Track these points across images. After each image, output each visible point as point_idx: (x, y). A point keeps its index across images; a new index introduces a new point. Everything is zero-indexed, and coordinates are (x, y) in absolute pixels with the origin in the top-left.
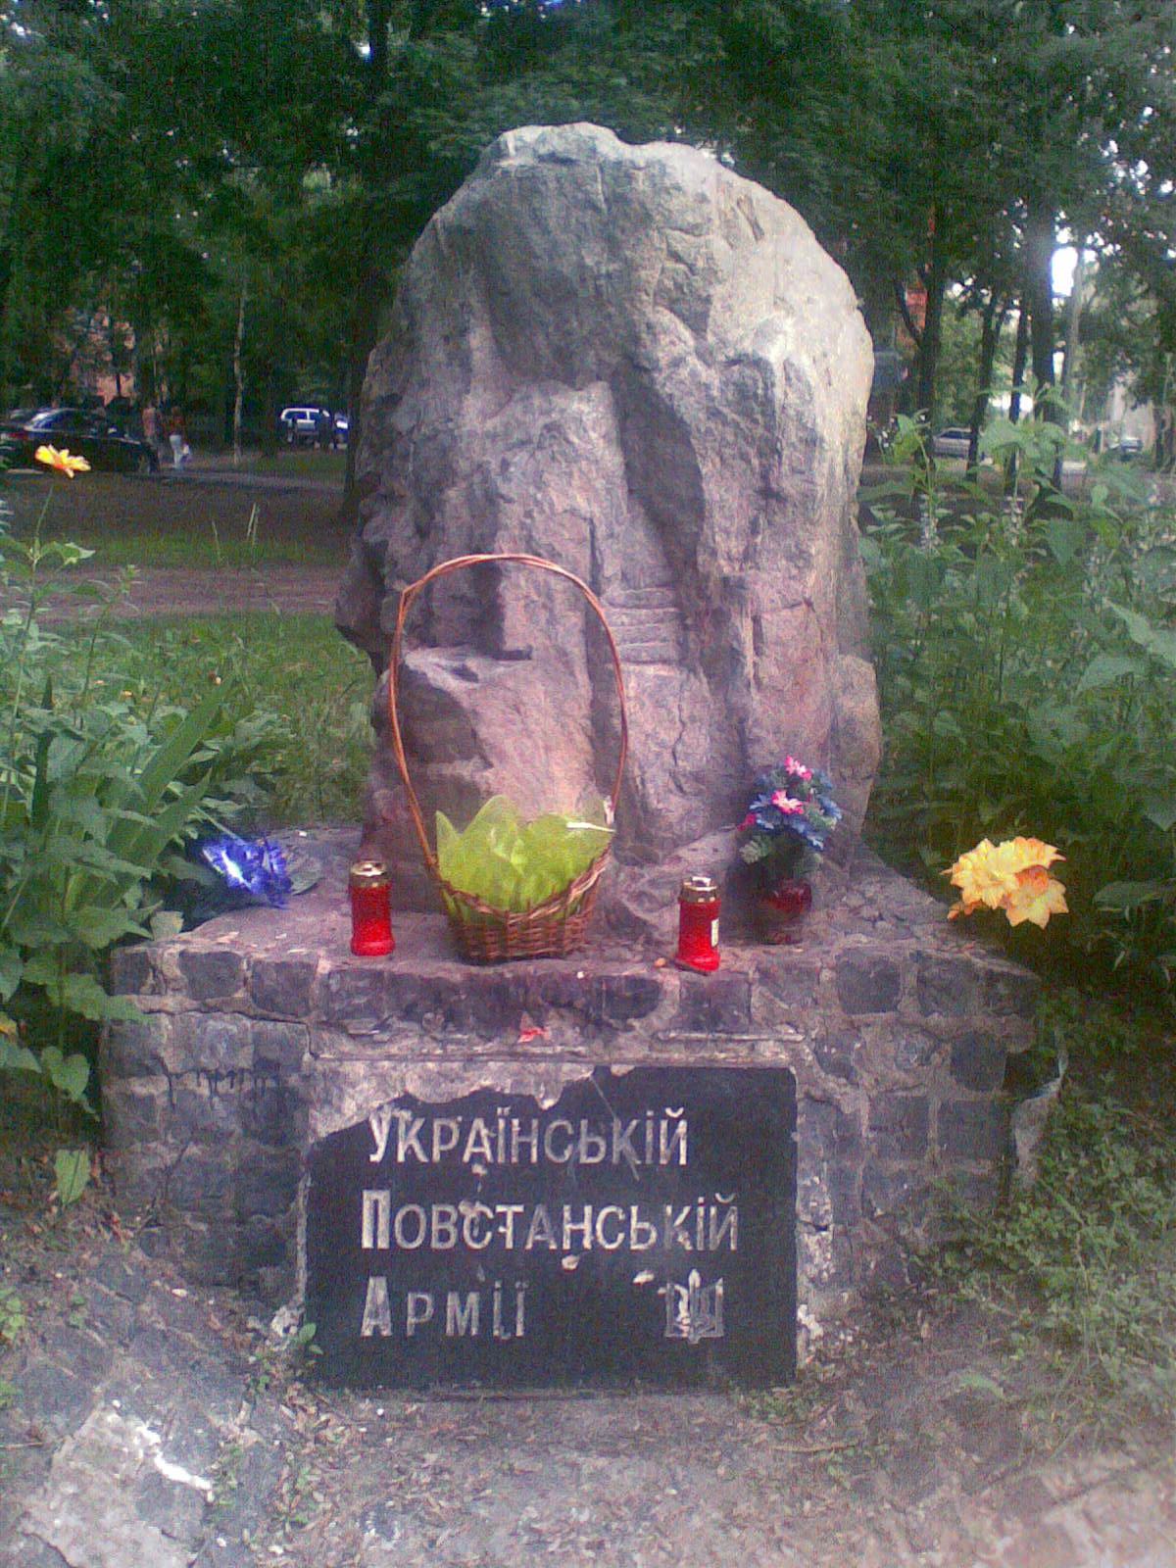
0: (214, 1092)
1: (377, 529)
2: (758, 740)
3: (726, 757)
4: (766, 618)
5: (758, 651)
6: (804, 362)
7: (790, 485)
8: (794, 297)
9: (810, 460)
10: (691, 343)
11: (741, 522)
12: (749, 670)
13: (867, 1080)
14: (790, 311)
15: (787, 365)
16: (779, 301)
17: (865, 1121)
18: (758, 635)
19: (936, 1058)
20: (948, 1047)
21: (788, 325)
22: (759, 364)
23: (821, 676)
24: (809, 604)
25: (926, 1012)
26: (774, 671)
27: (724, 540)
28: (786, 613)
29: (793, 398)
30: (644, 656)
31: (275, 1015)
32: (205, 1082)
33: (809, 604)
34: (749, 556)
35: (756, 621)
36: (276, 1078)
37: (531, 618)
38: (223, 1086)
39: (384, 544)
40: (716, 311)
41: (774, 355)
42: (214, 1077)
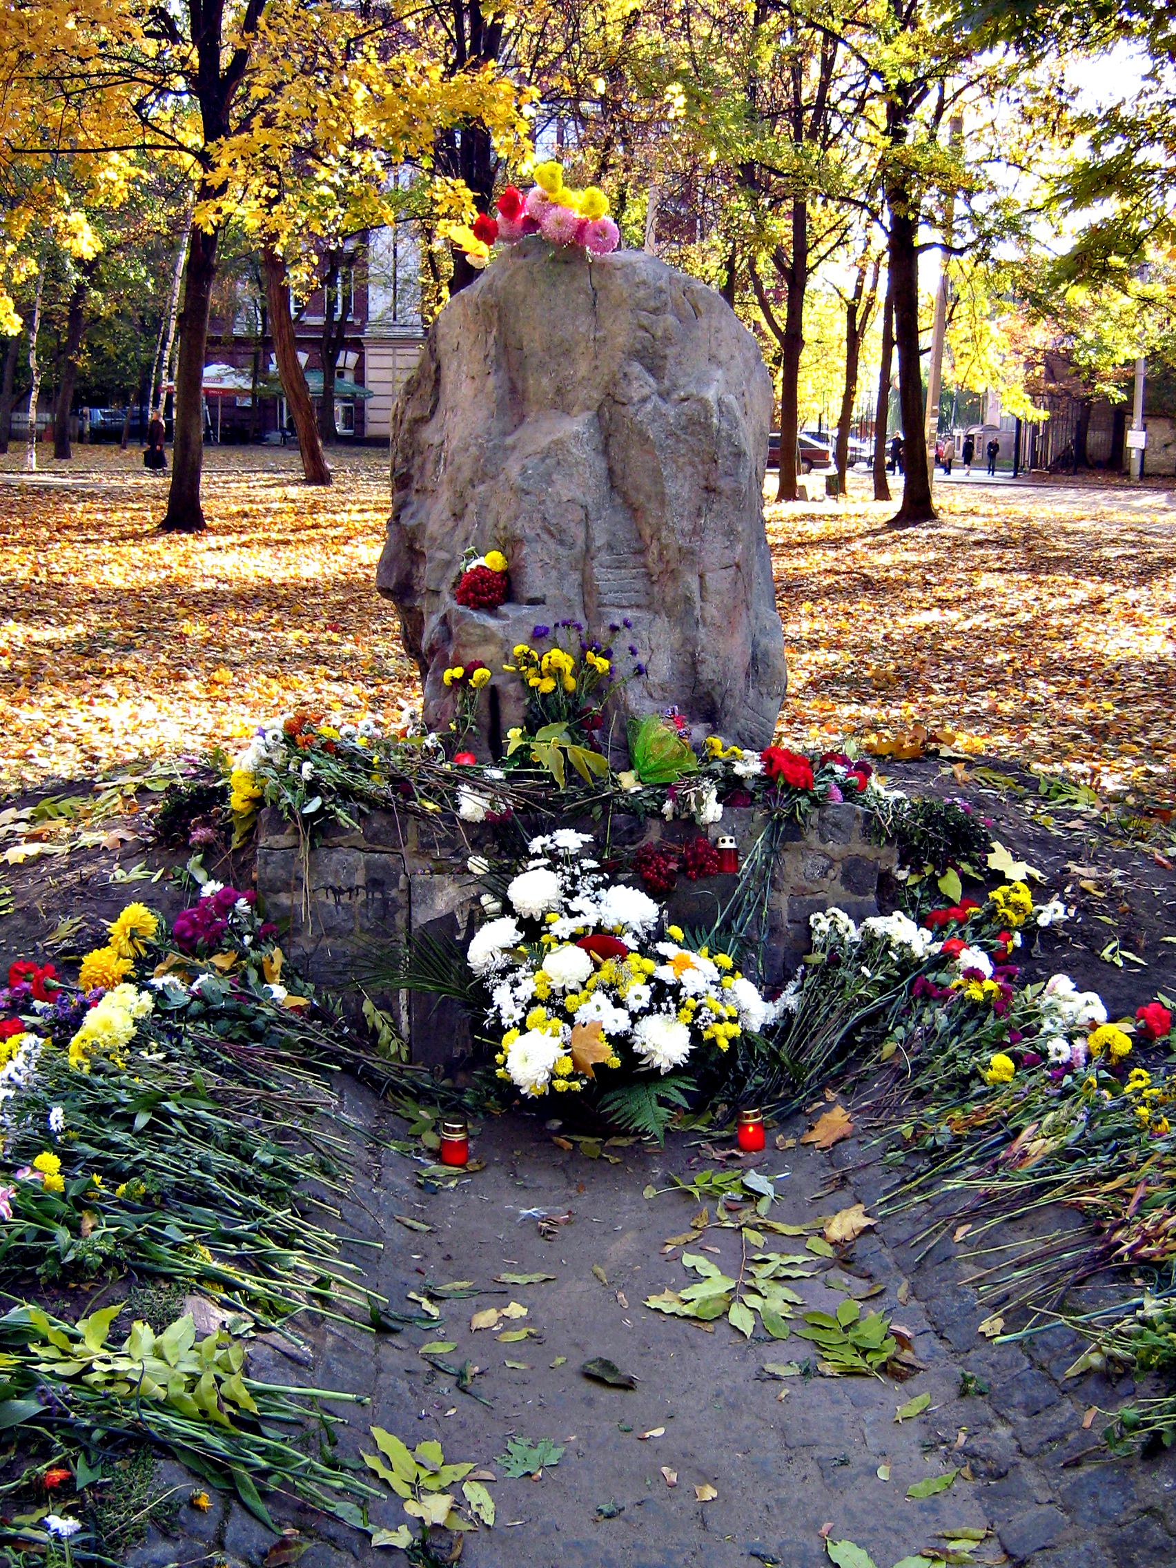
0: (338, 903)
1: (413, 516)
2: (703, 662)
3: (682, 673)
4: (708, 576)
5: (703, 599)
6: (730, 399)
7: (724, 484)
8: (723, 355)
9: (737, 468)
10: (654, 385)
11: (690, 507)
12: (697, 612)
13: (787, 887)
14: (720, 364)
15: (720, 402)
16: (712, 358)
17: (786, 917)
18: (702, 587)
19: (832, 873)
20: (839, 865)
21: (719, 374)
22: (703, 402)
23: (745, 621)
24: (738, 566)
25: (824, 841)
26: (715, 613)
27: (675, 524)
28: (723, 573)
29: (725, 425)
30: (625, 603)
31: (379, 848)
32: (331, 896)
33: (738, 566)
34: (697, 531)
35: (701, 577)
36: (382, 892)
37: (546, 574)
38: (344, 899)
39: (421, 527)
40: (670, 364)
41: (710, 395)
42: (337, 892)
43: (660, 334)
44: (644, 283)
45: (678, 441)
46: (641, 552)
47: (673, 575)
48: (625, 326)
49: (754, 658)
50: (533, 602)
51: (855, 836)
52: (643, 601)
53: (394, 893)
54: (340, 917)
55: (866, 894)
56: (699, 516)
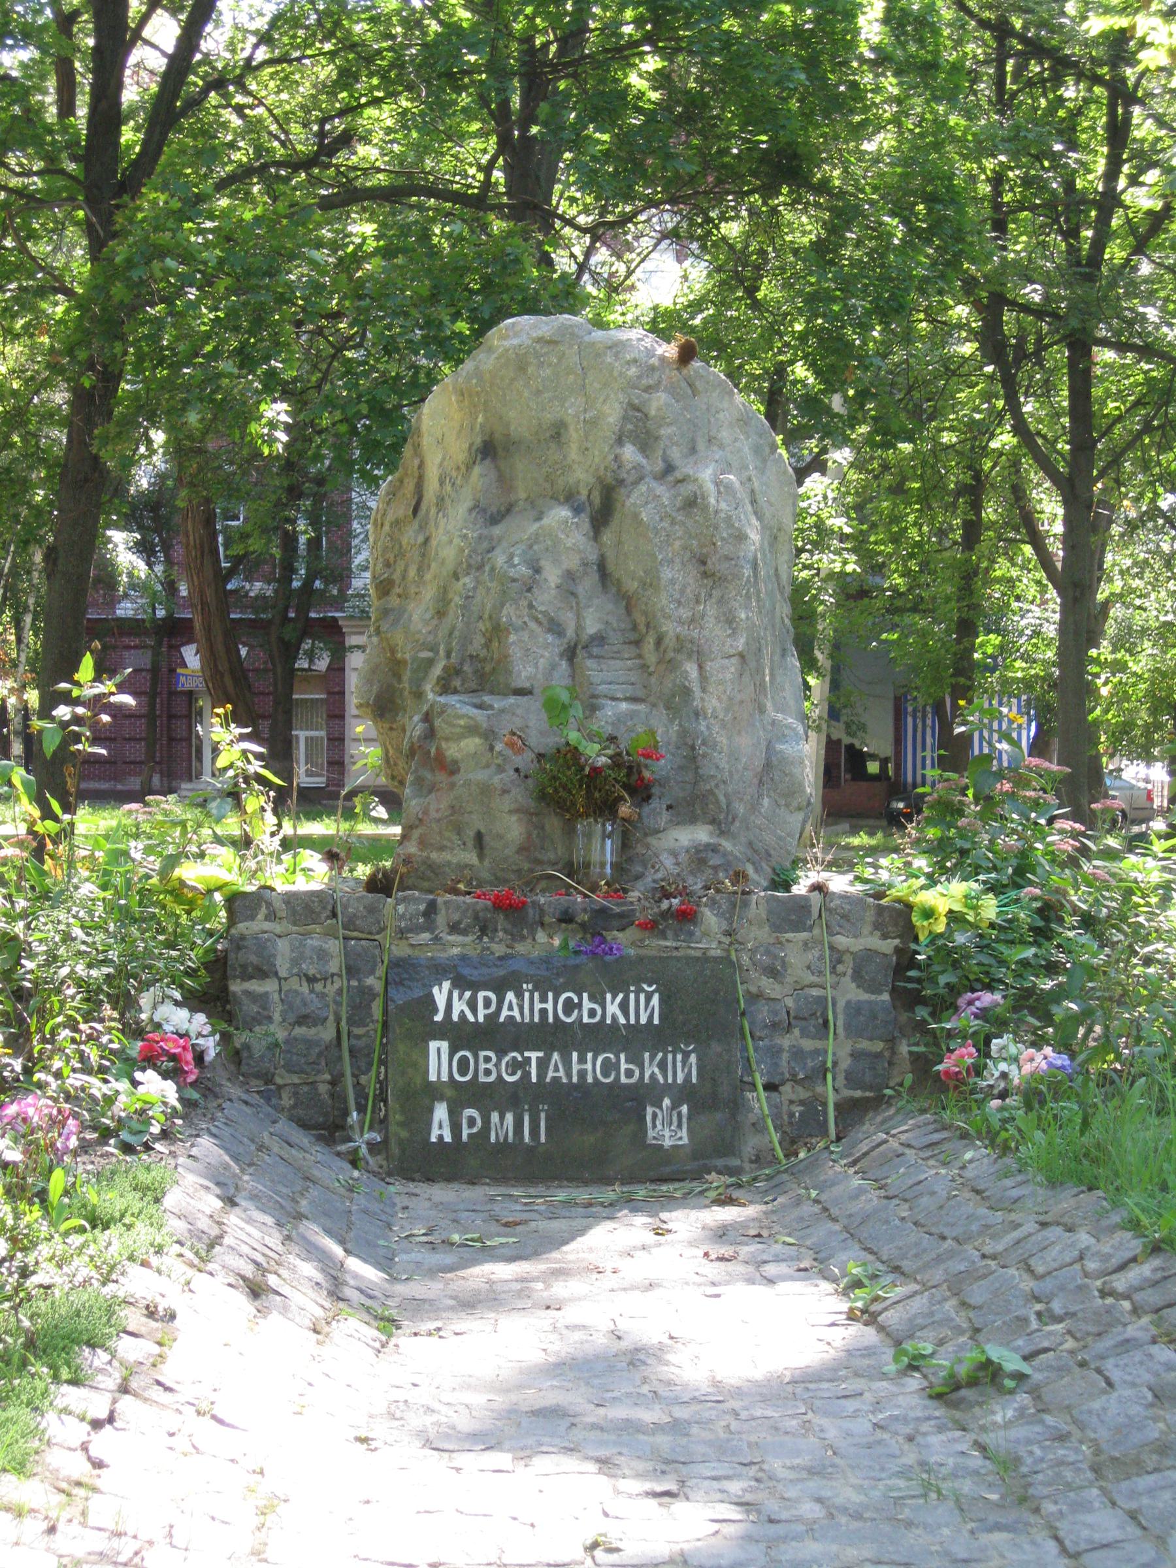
5: (704, 690)
38: (318, 987)
42: (311, 980)
43: (653, 413)
44: (635, 361)
45: (673, 523)
46: (637, 643)
47: (672, 665)
48: (616, 405)
49: (768, 766)
50: (520, 692)
51: (867, 929)
52: (640, 693)
53: (370, 981)
54: (315, 1003)
55: (880, 992)
56: (698, 602)
